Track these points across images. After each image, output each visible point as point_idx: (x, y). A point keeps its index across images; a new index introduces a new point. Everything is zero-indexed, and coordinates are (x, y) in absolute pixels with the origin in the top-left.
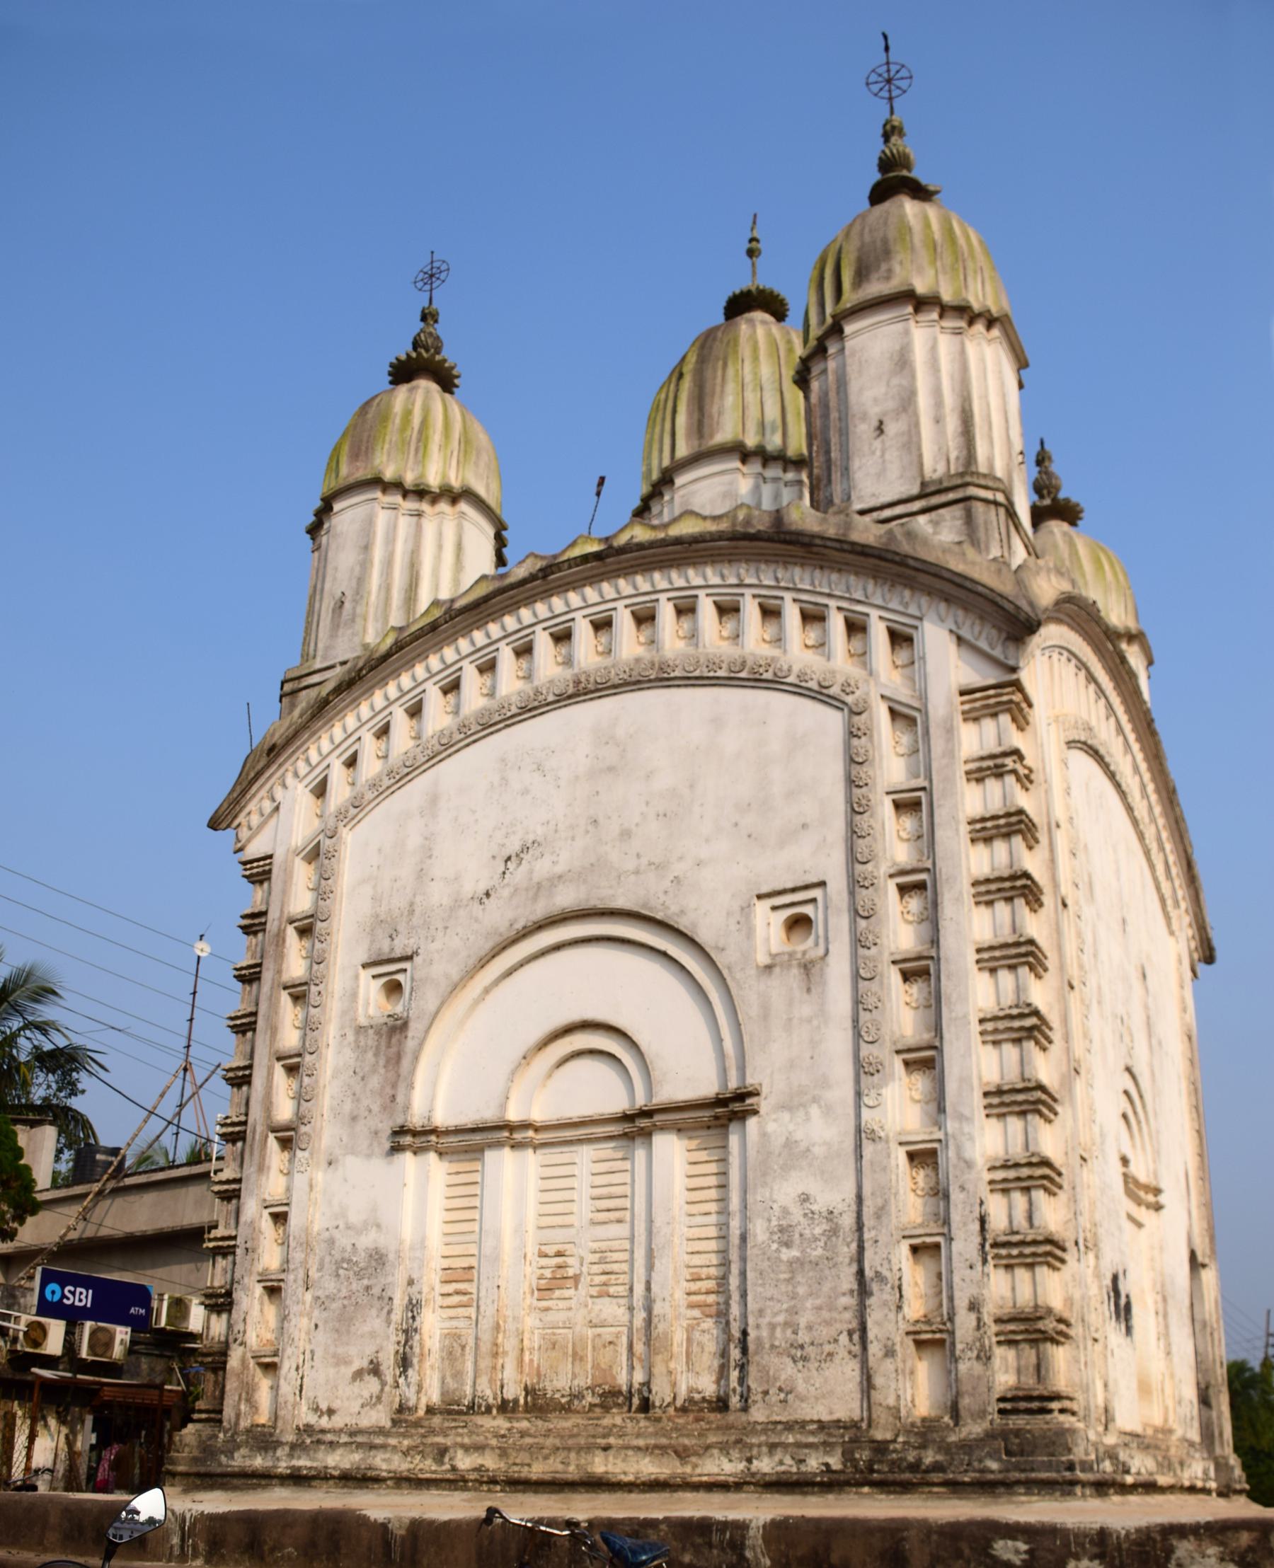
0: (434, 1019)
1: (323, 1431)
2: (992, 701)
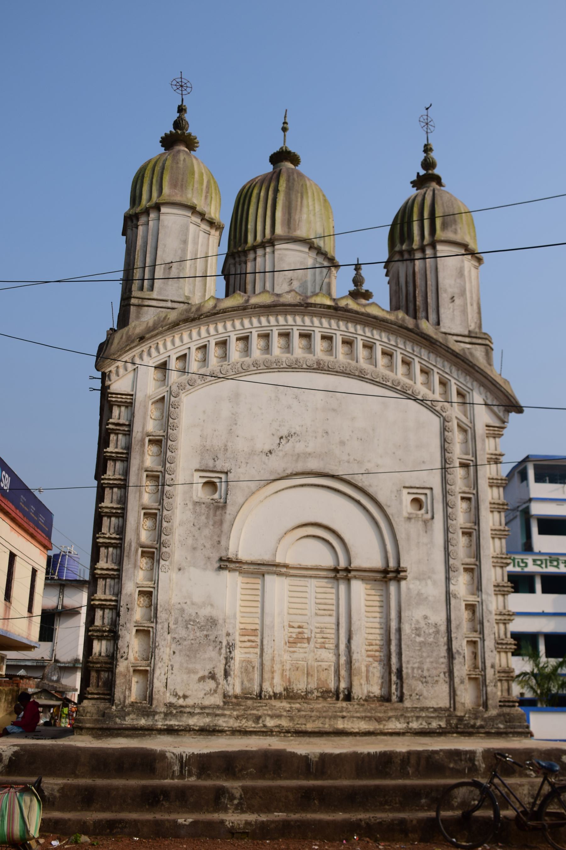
1: (182, 706)
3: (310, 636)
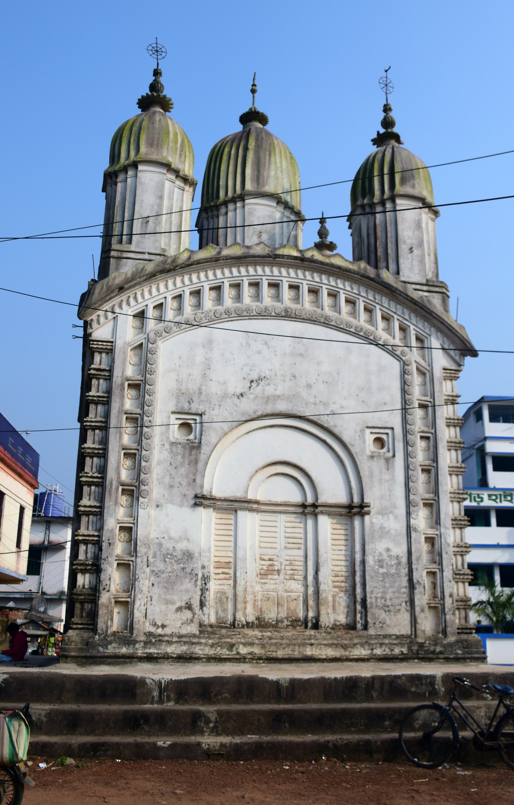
0: (215, 447)
1: (160, 635)
2: (453, 375)
3: (280, 568)
